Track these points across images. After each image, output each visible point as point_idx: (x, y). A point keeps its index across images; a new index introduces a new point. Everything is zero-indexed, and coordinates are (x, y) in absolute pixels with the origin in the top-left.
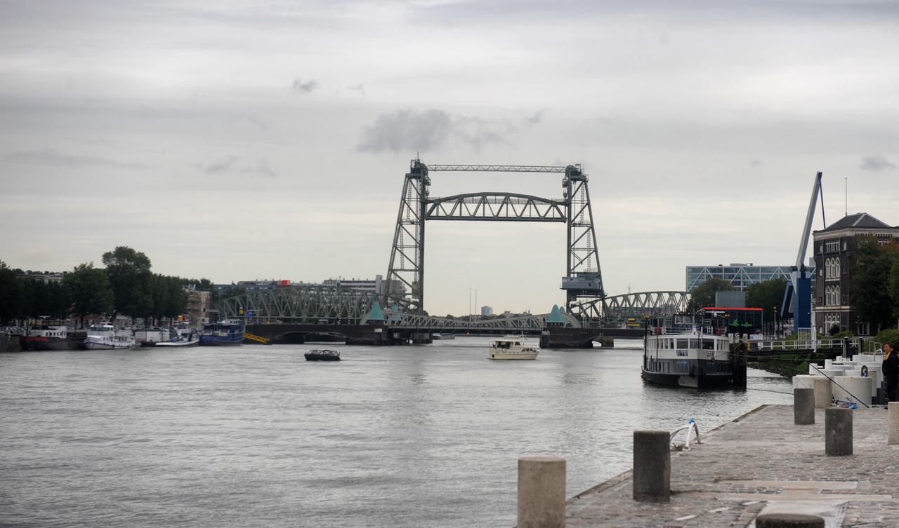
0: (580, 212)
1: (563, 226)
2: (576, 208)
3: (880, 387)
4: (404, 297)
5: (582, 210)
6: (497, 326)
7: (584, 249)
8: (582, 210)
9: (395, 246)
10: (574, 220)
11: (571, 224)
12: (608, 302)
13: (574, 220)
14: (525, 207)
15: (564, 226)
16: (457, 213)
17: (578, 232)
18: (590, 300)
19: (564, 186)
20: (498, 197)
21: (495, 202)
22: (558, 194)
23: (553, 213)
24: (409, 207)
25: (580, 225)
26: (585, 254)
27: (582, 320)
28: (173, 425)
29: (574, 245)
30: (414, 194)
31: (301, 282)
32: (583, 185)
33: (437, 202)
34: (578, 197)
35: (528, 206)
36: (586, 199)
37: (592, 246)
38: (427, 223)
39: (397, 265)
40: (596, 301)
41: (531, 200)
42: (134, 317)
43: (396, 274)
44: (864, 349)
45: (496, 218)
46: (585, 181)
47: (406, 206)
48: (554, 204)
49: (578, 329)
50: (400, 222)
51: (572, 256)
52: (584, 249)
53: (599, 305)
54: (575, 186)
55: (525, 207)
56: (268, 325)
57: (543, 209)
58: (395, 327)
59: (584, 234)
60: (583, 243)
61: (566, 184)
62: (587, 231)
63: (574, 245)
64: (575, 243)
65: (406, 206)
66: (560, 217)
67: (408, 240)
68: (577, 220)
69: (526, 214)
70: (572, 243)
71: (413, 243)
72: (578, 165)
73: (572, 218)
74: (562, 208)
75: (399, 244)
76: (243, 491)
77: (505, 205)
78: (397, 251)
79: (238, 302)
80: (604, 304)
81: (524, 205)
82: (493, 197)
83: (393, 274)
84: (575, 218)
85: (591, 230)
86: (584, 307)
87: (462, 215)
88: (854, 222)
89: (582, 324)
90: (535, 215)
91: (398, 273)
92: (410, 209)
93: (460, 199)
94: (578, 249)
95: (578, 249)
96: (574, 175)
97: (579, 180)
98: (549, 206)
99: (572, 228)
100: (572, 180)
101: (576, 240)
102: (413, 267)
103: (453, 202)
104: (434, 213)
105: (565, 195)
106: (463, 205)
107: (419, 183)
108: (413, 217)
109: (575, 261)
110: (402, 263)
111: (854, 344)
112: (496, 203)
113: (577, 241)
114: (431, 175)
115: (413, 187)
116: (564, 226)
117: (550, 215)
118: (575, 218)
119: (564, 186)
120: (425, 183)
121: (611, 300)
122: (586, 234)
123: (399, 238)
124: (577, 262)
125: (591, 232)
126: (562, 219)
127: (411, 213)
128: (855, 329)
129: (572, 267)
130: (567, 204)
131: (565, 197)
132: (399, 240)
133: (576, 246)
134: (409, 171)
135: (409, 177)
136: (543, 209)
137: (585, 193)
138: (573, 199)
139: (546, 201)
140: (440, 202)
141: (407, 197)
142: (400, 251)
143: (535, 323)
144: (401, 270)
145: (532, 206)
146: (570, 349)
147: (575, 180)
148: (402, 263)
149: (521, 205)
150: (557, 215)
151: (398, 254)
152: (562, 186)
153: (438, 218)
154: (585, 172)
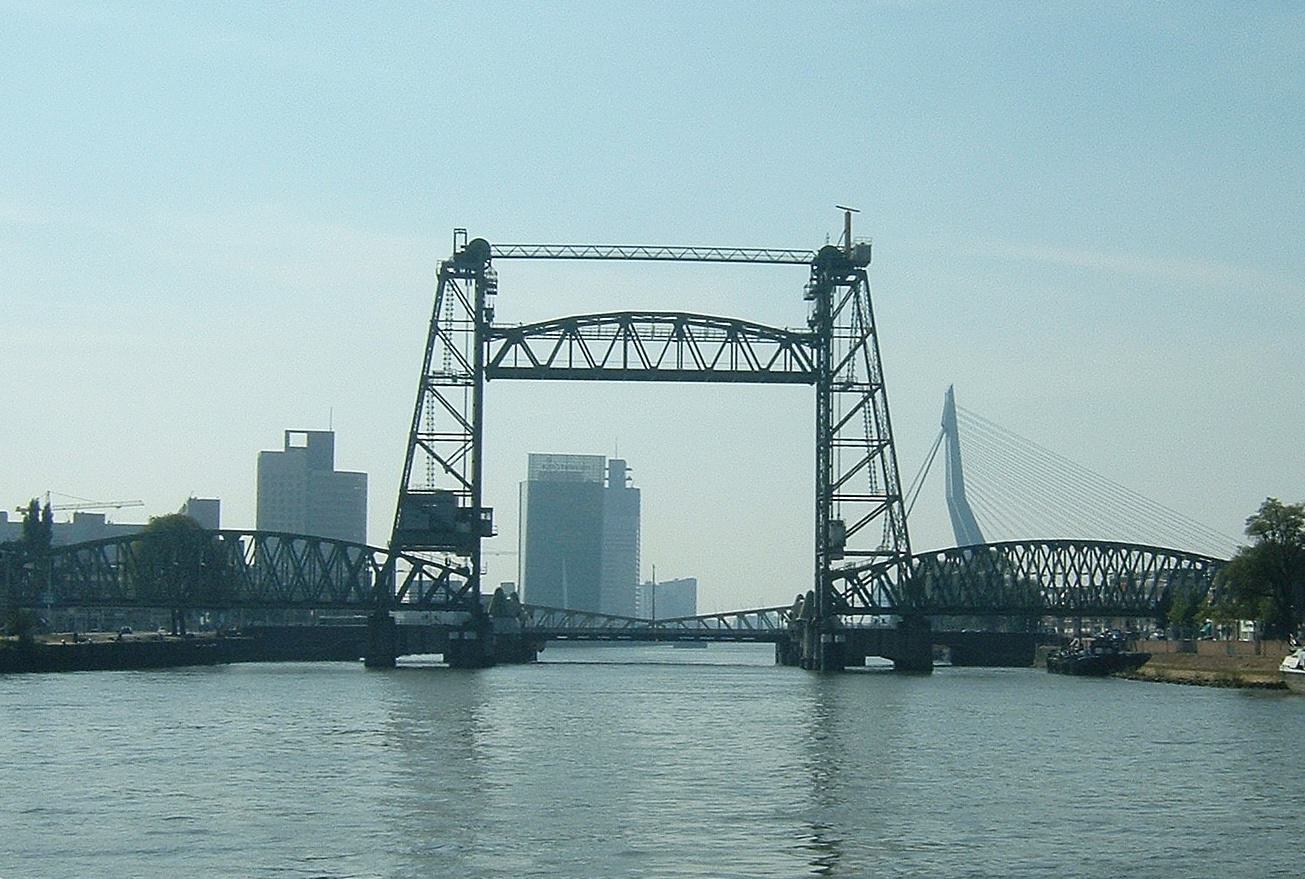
0: (848, 359)
4: (110, 582)
5: (852, 353)
8: (852, 353)
21: (653, 336)
22: (797, 316)
25: (847, 386)
29: (838, 427)
31: (619, 467)
41: (736, 330)
48: (787, 339)
50: (425, 384)
57: (765, 352)
59: (856, 410)
61: (820, 292)
62: (861, 405)
64: (841, 424)
66: (800, 370)
67: (442, 421)
69: (560, 362)
77: (566, 343)
87: (629, 367)
88: (849, 665)
90: (580, 363)
93: (569, 327)
108: (457, 368)
120: (486, 286)
128: (1264, 638)
133: (844, 490)
135: (444, 277)
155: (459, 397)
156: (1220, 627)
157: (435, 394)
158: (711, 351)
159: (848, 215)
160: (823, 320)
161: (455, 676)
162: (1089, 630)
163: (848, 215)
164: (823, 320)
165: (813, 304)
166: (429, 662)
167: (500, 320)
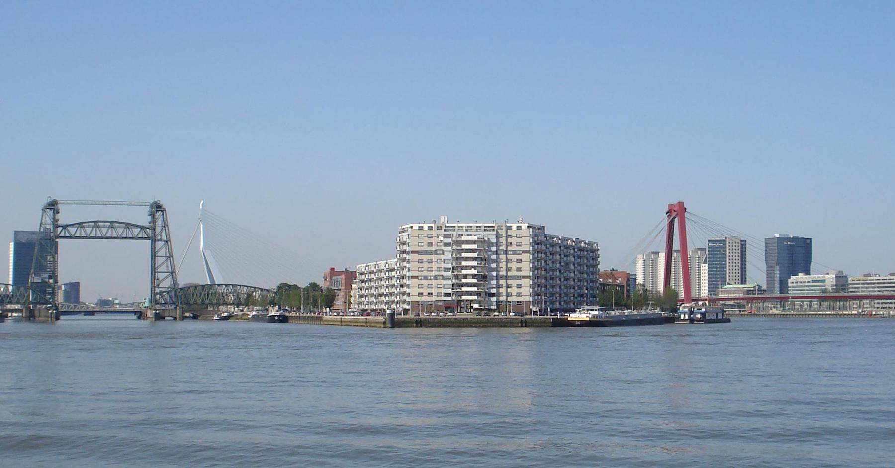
1: (148, 243)
14: (92, 230)
20: (90, 224)
21: (89, 226)
22: (145, 221)
25: (160, 241)
28: (718, 372)
33: (65, 227)
41: (128, 225)
42: (245, 299)
44: (245, 302)
46: (163, 210)
48: (142, 228)
55: (92, 230)
56: (623, 320)
57: (136, 231)
60: (162, 252)
61: (152, 215)
68: (159, 238)
76: (202, 350)
82: (87, 224)
93: (80, 225)
96: (157, 207)
98: (139, 229)
103: (75, 227)
111: (367, 306)
112: (104, 227)
114: (60, 206)
120: (57, 212)
126: (148, 238)
136: (136, 231)
139: (138, 226)
149: (87, 230)
154: (164, 206)
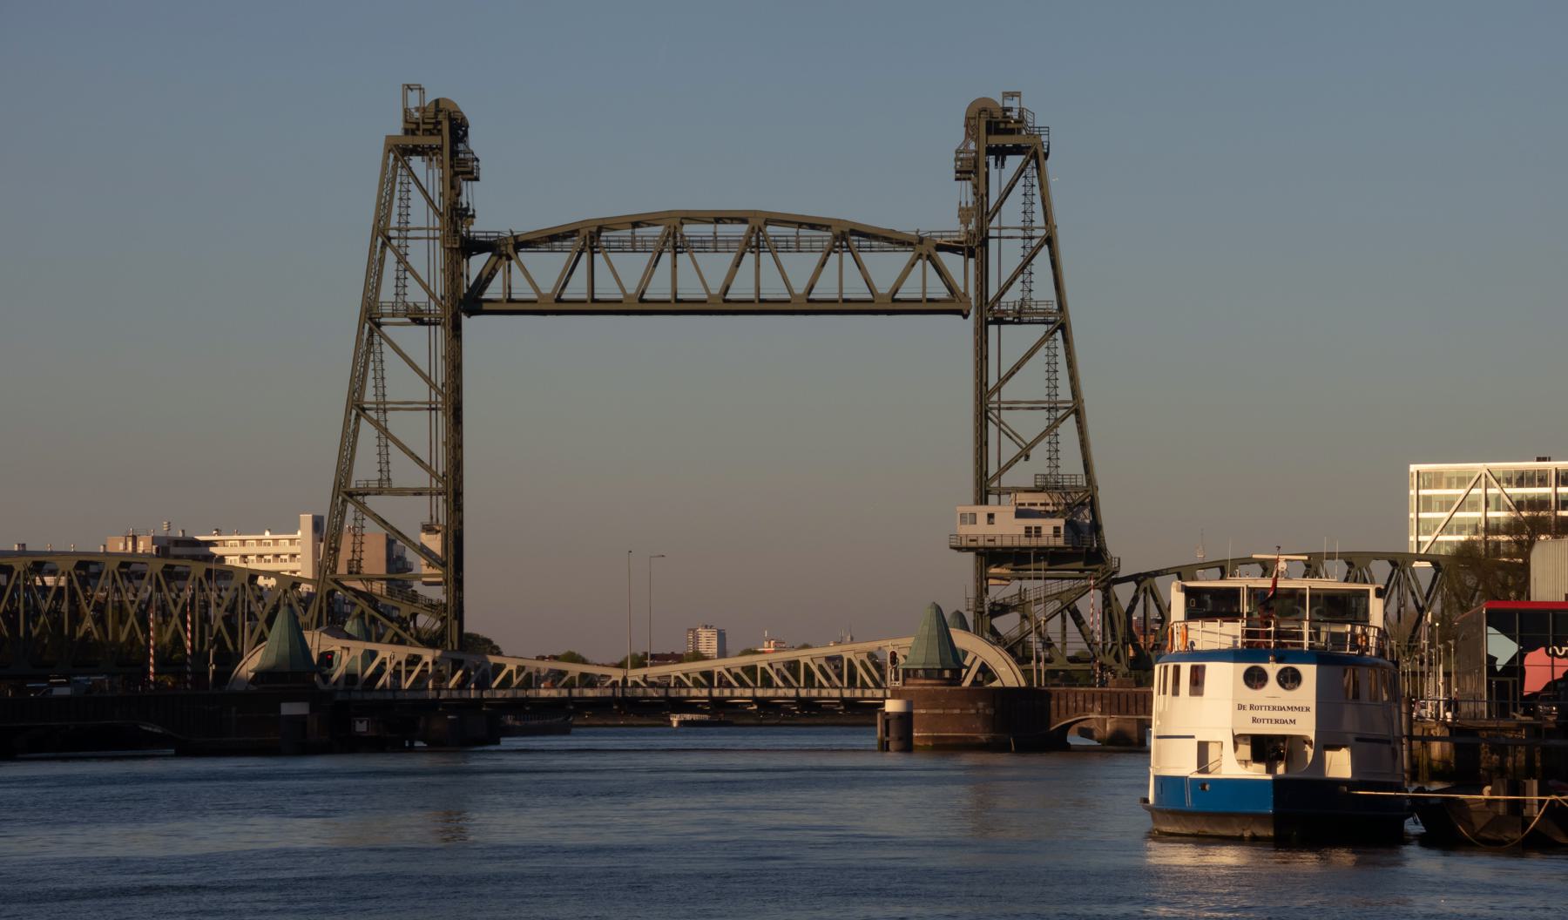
0: (1022, 269)
2: (1005, 256)
3: (228, 562)
5: (1028, 261)
6: (767, 682)
7: (1033, 406)
8: (1028, 261)
9: (357, 407)
10: (998, 298)
11: (990, 316)
12: (1124, 593)
13: (998, 298)
14: (823, 264)
15: (964, 329)
16: (577, 289)
17: (1012, 341)
18: (1055, 587)
19: (962, 174)
20: (723, 229)
21: (714, 245)
23: (923, 283)
24: (402, 259)
25: (1020, 316)
26: (1040, 420)
27: (1029, 659)
30: (420, 214)
32: (1031, 171)
33: (503, 249)
34: (1011, 214)
35: (834, 258)
36: (1039, 220)
37: (1065, 393)
38: (468, 323)
39: (365, 471)
40: (1085, 591)
43: (362, 507)
45: (725, 306)
46: (1036, 155)
47: (391, 257)
48: (924, 248)
49: (587, 687)
50: (372, 318)
51: (992, 429)
52: (1033, 406)
53: (1090, 606)
54: (1000, 175)
55: (823, 264)
57: (885, 267)
58: (358, 696)
60: (1030, 384)
61: (968, 170)
63: (998, 388)
65: (391, 257)
70: (993, 382)
71: (421, 392)
72: (1013, 95)
73: (993, 291)
74: (952, 262)
75: (369, 396)
77: (749, 258)
78: (363, 421)
79: (861, 676)
80: (1107, 601)
81: (818, 257)
82: (705, 230)
83: (350, 508)
84: (1002, 293)
85: (1059, 334)
86: (1039, 612)
89: (1027, 674)
90: (856, 289)
91: (371, 501)
92: (408, 268)
94: (1013, 406)
95: (1013, 406)
97: (1017, 150)
98: (905, 257)
99: (993, 329)
100: (990, 151)
101: (1004, 281)
102: (422, 479)
104: (494, 291)
105: (964, 214)
106: (598, 258)
107: (437, 172)
108: (416, 295)
109: (1001, 449)
110: (384, 463)
113: (1011, 373)
115: (413, 187)
116: (964, 329)
117: (910, 290)
118: (1002, 293)
119: (962, 174)
120: (462, 170)
121: (1132, 586)
122: (1043, 351)
123: (371, 374)
124: (1010, 450)
125: (1060, 343)
126: (951, 307)
127: (411, 281)
129: (992, 470)
130: (975, 247)
131: (966, 223)
132: (370, 382)
133: (1008, 393)
134: (397, 128)
135: (401, 151)
136: (885, 267)
137: (1037, 199)
138: (995, 223)
140: (516, 249)
141: (394, 222)
142: (376, 424)
143: (860, 670)
144: (379, 492)
145: (847, 257)
146: (1064, 304)
147: (1001, 153)
148: (384, 463)
150: (938, 290)
151: (367, 432)
152: (953, 175)
153: (513, 307)
155: (419, 342)
156: (132, 689)
157: (383, 336)
158: (796, 269)
159: (976, 658)
160: (982, 212)
161: (879, 753)
162: (152, 678)
163: (976, 658)
164: (982, 212)
165: (967, 186)
166: (492, 760)
167: (481, 226)
